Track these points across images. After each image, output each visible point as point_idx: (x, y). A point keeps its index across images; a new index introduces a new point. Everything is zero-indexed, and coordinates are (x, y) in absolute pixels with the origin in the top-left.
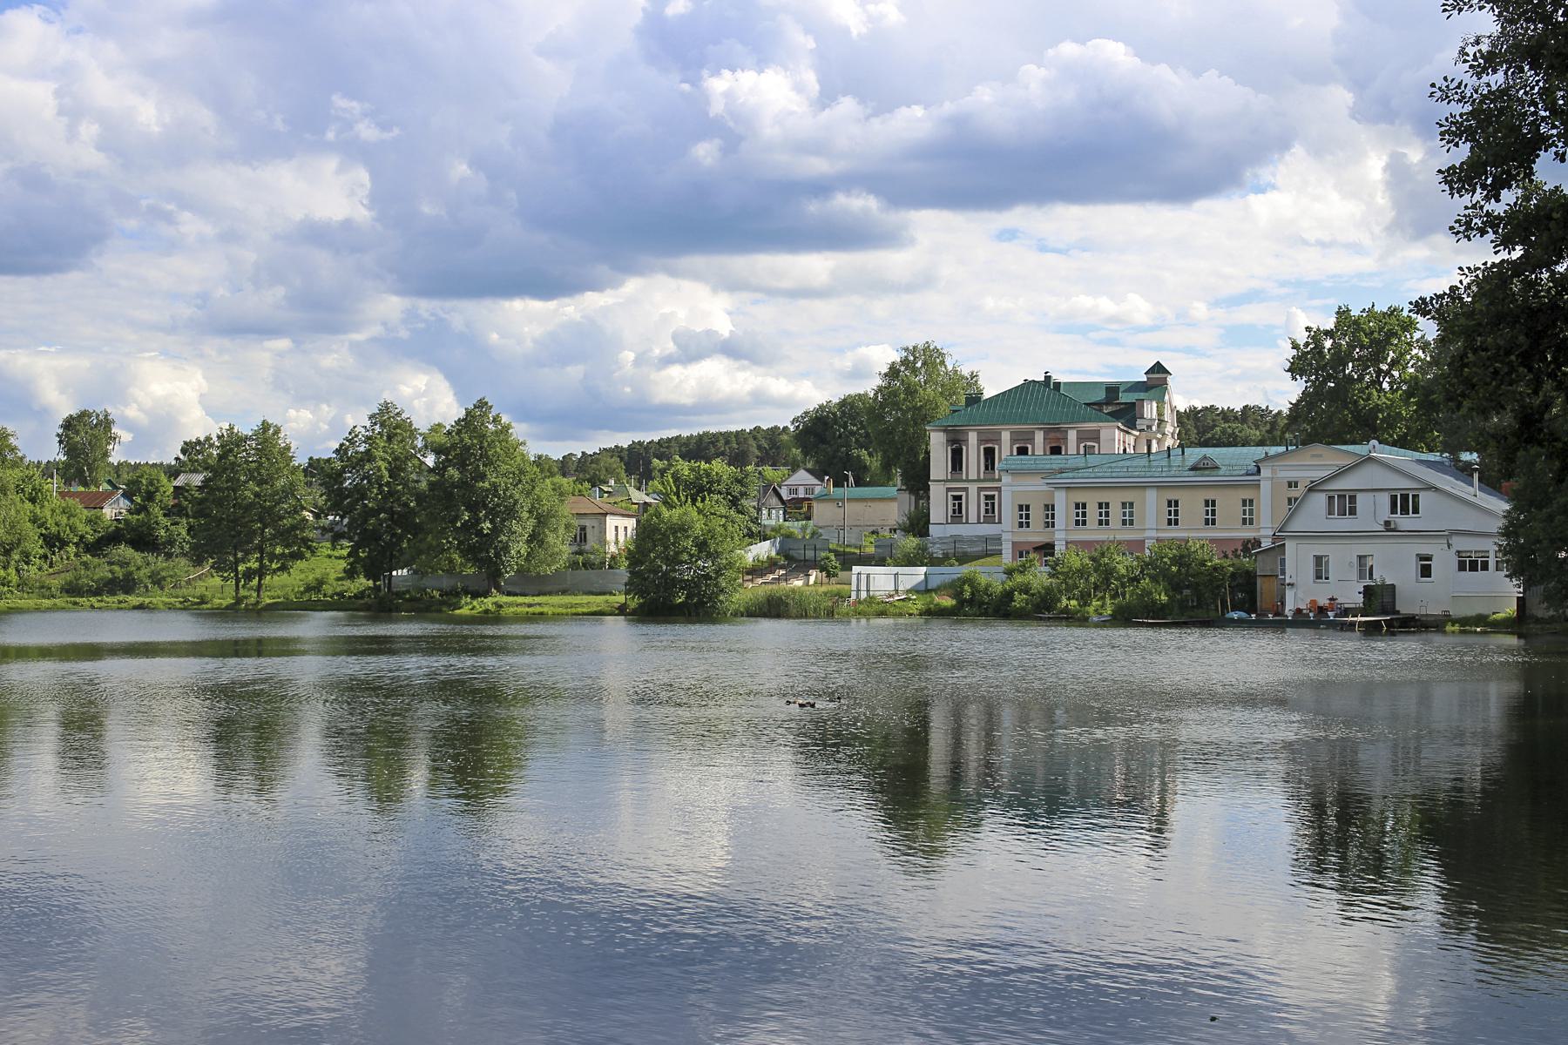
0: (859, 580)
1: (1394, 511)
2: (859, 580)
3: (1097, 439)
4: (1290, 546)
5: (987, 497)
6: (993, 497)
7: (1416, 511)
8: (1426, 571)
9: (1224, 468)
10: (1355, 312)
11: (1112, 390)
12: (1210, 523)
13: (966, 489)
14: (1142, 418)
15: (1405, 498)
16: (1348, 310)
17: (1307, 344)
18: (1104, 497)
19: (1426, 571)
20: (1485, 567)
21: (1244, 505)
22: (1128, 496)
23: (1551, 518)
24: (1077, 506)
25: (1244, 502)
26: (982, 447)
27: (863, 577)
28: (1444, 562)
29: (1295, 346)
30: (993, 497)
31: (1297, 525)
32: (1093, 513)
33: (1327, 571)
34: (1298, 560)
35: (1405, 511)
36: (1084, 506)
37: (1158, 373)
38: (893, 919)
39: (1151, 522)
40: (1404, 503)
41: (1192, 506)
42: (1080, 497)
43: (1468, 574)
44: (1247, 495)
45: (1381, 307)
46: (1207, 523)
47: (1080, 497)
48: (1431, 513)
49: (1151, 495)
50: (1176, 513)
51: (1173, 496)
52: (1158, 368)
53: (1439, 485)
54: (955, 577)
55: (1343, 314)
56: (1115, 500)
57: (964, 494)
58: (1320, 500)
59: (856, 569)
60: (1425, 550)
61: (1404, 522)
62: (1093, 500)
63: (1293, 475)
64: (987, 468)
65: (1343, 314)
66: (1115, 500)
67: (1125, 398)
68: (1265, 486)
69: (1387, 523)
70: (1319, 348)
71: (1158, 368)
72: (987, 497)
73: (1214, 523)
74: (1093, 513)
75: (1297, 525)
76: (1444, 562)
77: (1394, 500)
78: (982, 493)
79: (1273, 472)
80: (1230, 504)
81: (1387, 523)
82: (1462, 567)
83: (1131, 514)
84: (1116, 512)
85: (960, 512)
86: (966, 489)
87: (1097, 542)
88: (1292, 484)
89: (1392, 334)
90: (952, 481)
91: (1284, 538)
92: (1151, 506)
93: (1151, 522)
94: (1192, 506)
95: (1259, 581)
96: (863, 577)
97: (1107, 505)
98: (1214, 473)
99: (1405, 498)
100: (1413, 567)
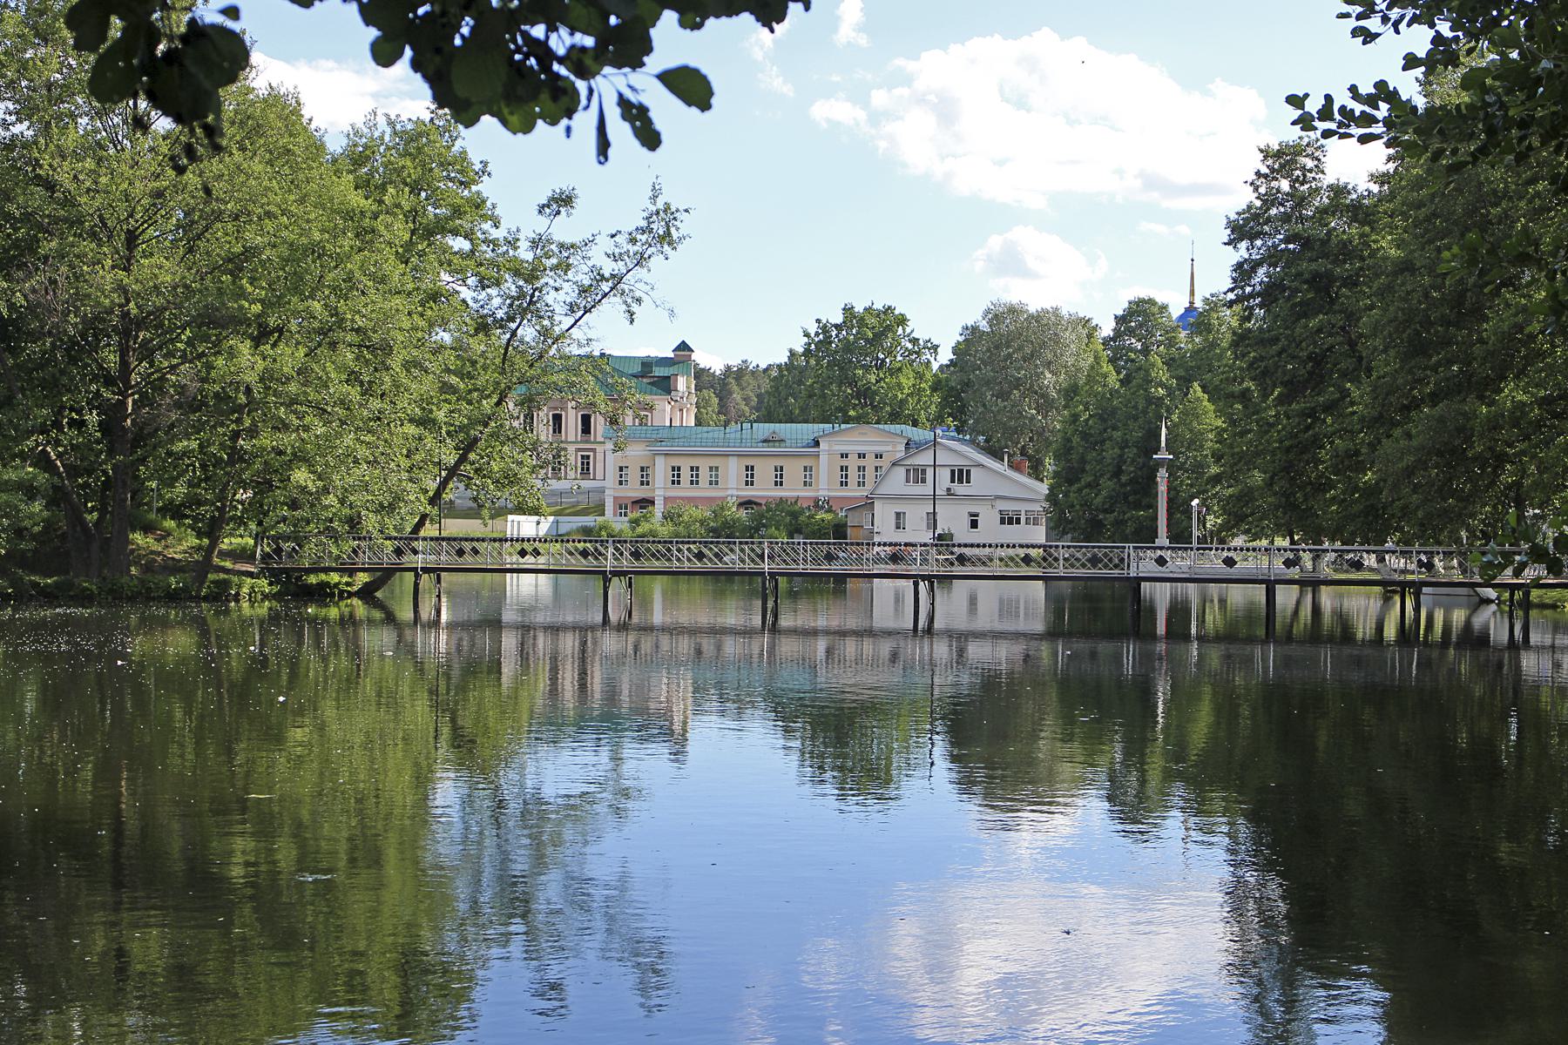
0: (512, 526)
1: (953, 481)
2: (512, 526)
3: (651, 409)
4: (877, 505)
5: (583, 457)
6: (588, 457)
7: (968, 482)
8: (974, 524)
9: (788, 441)
10: (859, 308)
11: (647, 364)
12: (780, 484)
13: (594, 450)
14: (676, 390)
15: (961, 471)
16: (853, 307)
17: (817, 334)
18: (695, 462)
19: (974, 524)
20: (1018, 521)
21: (747, 470)
22: (714, 462)
23: (1080, 490)
24: (673, 469)
25: (805, 468)
26: (551, 414)
27: (516, 524)
28: (989, 517)
29: (807, 335)
30: (588, 457)
31: (883, 490)
32: (686, 475)
33: (904, 524)
34: (883, 516)
35: (961, 481)
36: (679, 469)
37: (684, 350)
38: (775, 726)
39: (732, 483)
40: (960, 475)
41: (765, 470)
42: (676, 462)
43: (1006, 526)
44: (807, 462)
45: (878, 306)
46: (776, 485)
47: (676, 462)
48: (979, 483)
49: (733, 462)
50: (752, 476)
51: (750, 462)
52: (683, 347)
53: (985, 464)
54: (580, 524)
55: (848, 310)
56: (704, 465)
57: (591, 454)
58: (901, 472)
59: (510, 517)
60: (974, 510)
61: (960, 489)
62: (685, 465)
63: (844, 449)
64: (554, 432)
65: (848, 310)
66: (704, 465)
67: (659, 372)
68: (823, 458)
69: (949, 489)
70: (827, 341)
71: (683, 347)
72: (583, 457)
73: (781, 485)
74: (686, 475)
75: (883, 490)
76: (989, 517)
77: (953, 472)
78: (580, 453)
79: (830, 446)
80: (793, 470)
81: (949, 489)
82: (1002, 522)
83: (717, 476)
84: (704, 475)
85: (588, 469)
86: (594, 450)
87: (720, 498)
88: (844, 456)
89: (889, 328)
90: (581, 442)
91: (872, 498)
92: (733, 471)
93: (732, 483)
94: (765, 470)
95: (849, 529)
96: (516, 524)
97: (698, 468)
98: (783, 444)
99: (961, 471)
100: (966, 521)
